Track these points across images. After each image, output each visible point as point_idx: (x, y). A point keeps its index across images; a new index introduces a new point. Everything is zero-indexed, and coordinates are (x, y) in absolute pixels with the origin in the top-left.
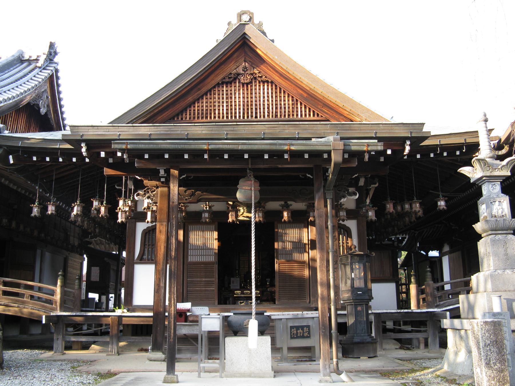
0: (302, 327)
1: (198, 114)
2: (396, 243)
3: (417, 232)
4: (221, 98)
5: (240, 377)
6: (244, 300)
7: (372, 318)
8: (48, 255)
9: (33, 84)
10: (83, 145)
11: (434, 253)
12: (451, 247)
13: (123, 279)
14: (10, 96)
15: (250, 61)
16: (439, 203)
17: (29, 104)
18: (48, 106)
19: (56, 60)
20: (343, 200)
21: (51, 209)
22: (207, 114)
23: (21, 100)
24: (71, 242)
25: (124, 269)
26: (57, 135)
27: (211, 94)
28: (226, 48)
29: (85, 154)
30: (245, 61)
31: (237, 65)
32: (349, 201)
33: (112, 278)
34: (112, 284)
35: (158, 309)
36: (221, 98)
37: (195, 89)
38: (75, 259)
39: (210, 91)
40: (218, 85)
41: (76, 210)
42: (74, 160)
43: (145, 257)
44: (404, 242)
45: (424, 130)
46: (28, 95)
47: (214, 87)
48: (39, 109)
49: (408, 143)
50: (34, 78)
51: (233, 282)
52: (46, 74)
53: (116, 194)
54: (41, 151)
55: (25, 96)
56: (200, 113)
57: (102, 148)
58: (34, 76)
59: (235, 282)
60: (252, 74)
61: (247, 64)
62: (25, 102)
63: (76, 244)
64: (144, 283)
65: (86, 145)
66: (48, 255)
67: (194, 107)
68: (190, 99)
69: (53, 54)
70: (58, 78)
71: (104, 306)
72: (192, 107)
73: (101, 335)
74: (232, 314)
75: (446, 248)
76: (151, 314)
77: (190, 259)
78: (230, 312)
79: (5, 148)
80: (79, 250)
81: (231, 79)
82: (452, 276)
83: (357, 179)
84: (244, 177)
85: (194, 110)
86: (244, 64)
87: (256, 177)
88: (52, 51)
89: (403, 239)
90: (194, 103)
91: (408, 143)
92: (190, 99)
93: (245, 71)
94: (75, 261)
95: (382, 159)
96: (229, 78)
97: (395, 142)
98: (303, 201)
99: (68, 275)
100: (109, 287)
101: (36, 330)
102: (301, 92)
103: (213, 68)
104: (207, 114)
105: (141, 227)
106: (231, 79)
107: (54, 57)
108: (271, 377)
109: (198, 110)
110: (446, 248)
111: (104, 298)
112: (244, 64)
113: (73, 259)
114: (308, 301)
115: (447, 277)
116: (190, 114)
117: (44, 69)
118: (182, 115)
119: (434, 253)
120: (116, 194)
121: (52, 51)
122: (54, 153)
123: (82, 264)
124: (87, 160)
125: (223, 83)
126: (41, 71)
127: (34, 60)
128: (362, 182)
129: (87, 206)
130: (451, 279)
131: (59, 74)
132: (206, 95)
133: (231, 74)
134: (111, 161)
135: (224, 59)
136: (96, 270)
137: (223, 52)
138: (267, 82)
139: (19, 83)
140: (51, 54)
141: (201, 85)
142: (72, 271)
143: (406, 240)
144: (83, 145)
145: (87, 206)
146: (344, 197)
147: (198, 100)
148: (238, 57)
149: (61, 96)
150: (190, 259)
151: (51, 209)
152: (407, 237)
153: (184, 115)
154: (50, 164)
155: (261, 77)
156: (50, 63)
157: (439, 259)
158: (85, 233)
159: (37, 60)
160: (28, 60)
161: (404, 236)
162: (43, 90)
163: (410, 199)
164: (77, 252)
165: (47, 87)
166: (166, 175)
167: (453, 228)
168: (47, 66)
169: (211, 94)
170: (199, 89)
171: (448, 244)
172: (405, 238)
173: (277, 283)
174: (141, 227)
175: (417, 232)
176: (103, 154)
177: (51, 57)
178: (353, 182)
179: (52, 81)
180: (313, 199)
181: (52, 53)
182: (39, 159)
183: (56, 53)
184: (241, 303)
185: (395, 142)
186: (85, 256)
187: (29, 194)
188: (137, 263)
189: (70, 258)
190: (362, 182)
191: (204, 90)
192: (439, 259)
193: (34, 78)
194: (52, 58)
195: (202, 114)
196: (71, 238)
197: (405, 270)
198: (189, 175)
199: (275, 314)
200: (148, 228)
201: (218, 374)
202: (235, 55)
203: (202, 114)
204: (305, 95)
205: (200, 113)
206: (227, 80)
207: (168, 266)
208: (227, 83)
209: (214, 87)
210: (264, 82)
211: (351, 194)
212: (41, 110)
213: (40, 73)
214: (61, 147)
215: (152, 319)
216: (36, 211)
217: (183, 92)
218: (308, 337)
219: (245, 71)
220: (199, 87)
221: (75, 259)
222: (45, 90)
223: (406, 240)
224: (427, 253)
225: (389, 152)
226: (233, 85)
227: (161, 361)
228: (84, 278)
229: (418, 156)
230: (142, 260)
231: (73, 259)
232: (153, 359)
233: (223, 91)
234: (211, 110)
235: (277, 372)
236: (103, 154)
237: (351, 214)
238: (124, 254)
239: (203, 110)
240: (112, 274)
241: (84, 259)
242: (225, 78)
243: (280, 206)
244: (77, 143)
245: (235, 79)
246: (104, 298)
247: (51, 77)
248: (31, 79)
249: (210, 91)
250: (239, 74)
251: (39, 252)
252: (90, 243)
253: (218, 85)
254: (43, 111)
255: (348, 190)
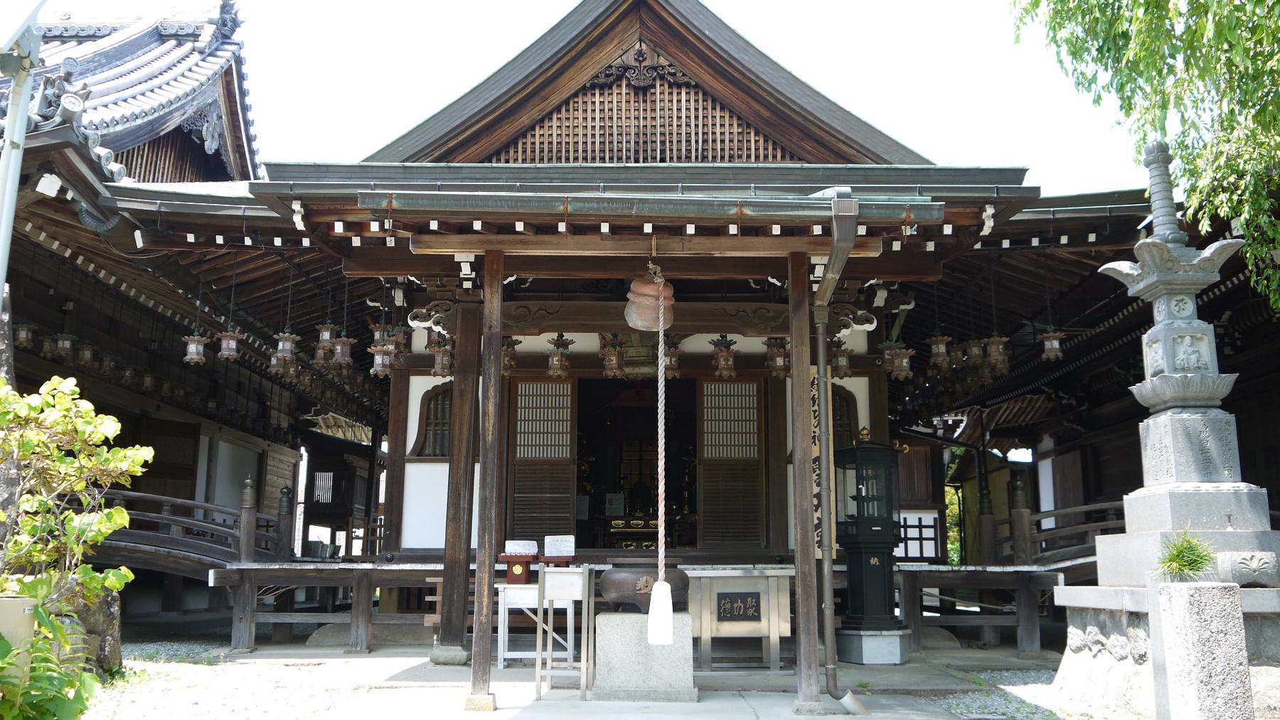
0: (744, 596)
1: (542, 151)
2: (940, 432)
3: (987, 411)
4: (589, 119)
5: (624, 699)
6: (633, 541)
7: (899, 579)
8: (224, 449)
9: (186, 86)
10: (296, 206)
11: (1021, 455)
12: (1058, 441)
13: (382, 499)
14: (137, 111)
15: (651, 41)
16: (1047, 344)
17: (179, 129)
18: (221, 136)
19: (236, 37)
20: (844, 333)
21: (229, 346)
22: (559, 151)
23: (162, 120)
24: (274, 421)
25: (383, 476)
26: (238, 189)
27: (567, 111)
28: (601, 10)
29: (300, 226)
30: (641, 41)
31: (625, 48)
32: (855, 336)
33: (358, 493)
34: (359, 507)
35: (456, 558)
36: (589, 119)
37: (536, 100)
38: (282, 457)
39: (567, 102)
40: (584, 90)
41: (285, 346)
42: (278, 242)
43: (428, 450)
44: (959, 431)
45: (1025, 184)
46: (177, 109)
47: (576, 95)
48: (203, 141)
49: (990, 210)
50: (187, 73)
51: (611, 503)
52: (214, 65)
53: (368, 318)
54: (206, 222)
55: (171, 113)
56: (546, 150)
57: (339, 214)
58: (190, 70)
59: (616, 503)
60: (655, 69)
61: (644, 46)
62: (171, 125)
63: (285, 424)
64: (426, 503)
65: (293, 554)
66: (224, 450)
67: (534, 136)
68: (524, 119)
69: (229, 24)
70: (241, 77)
71: (342, 553)
72: (529, 136)
73: (333, 611)
74: (608, 567)
75: (1048, 443)
76: (440, 567)
77: (521, 453)
78: (605, 563)
79: (126, 215)
80: (290, 437)
81: (611, 79)
82: (1060, 500)
83: (872, 291)
84: (641, 276)
85: (533, 143)
86: (637, 46)
87: (669, 281)
88: (227, 17)
89: (957, 424)
90: (533, 128)
91: (990, 210)
92: (524, 119)
93: (640, 62)
94: (281, 461)
95: (930, 246)
96: (607, 76)
97: (961, 210)
98: (759, 334)
99: (268, 477)
100: (351, 514)
101: (198, 603)
102: (756, 106)
103: (573, 53)
104: (559, 151)
105: (420, 386)
106: (611, 79)
107: (233, 31)
108: (691, 700)
109: (542, 143)
110: (1048, 443)
111: (341, 537)
112: (637, 46)
113: (279, 457)
114: (763, 544)
115: (1047, 502)
116: (524, 152)
117: (210, 55)
118: (508, 152)
119: (1021, 455)
120: (368, 318)
121: (227, 17)
122: (234, 228)
123: (296, 467)
124: (306, 242)
125: (593, 87)
126: (203, 60)
127: (188, 35)
128: (880, 299)
129: (307, 343)
130: (1056, 507)
131: (245, 69)
132: (559, 111)
133: (610, 67)
134: (356, 242)
135: (596, 33)
136: (325, 481)
137: (596, 20)
138: (687, 85)
139: (156, 82)
140: (225, 25)
141: (547, 91)
142: (275, 481)
143: (962, 425)
144: (296, 206)
145: (307, 343)
146: (846, 326)
147: (541, 121)
148: (626, 30)
149: (248, 100)
150: (521, 453)
151: (229, 346)
152: (965, 418)
153: (512, 153)
154: (224, 251)
155: (674, 75)
156: (223, 43)
157: (1032, 469)
158: (303, 403)
159: (195, 37)
160: (175, 36)
161: (959, 418)
162: (210, 101)
163: (983, 333)
164: (284, 442)
165: (218, 93)
166: (473, 275)
167: (1065, 401)
168: (217, 49)
169: (567, 111)
170: (545, 99)
171: (1051, 436)
172: (961, 421)
173: (700, 506)
174: (420, 386)
175: (987, 411)
176: (339, 228)
177: (226, 30)
178: (862, 299)
179: (231, 82)
180: (786, 328)
181: (226, 27)
182: (201, 240)
183: (236, 24)
184: (627, 546)
185: (961, 210)
186: (303, 450)
187: (183, 318)
188: (410, 461)
189: (270, 453)
190: (880, 299)
191: (555, 100)
192: (1032, 469)
193: (187, 73)
194: (228, 33)
195: (550, 151)
196: (274, 413)
197: (957, 489)
198: (524, 275)
199: (693, 572)
200: (435, 388)
201: (578, 693)
202: (620, 27)
203: (550, 151)
204: (766, 114)
205: (546, 150)
206: (602, 80)
207: (477, 467)
208: (602, 87)
209: (576, 95)
210: (679, 86)
211: (860, 321)
212: (206, 144)
213: (201, 63)
214: (248, 213)
215: (440, 580)
216: (194, 350)
217: (510, 104)
218: (757, 618)
219: (640, 62)
220: (543, 94)
221: (282, 457)
222: (215, 101)
223: (962, 425)
224: (1005, 453)
225: (948, 230)
226: (615, 91)
227: (459, 664)
228: (301, 497)
229: (1006, 244)
230: (421, 454)
231: (279, 457)
232: (441, 660)
233: (594, 103)
234: (568, 143)
235: (705, 690)
236: (339, 228)
237: (858, 365)
238: (385, 447)
239: (550, 143)
240: (360, 487)
241: (301, 456)
242: (597, 76)
243: (712, 342)
244: (282, 202)
245: (619, 78)
246: (341, 537)
247: (228, 72)
248: (183, 75)
249: (567, 102)
250: (626, 68)
251: (204, 441)
252: (315, 425)
253: (584, 90)
254: (210, 146)
255: (854, 313)
